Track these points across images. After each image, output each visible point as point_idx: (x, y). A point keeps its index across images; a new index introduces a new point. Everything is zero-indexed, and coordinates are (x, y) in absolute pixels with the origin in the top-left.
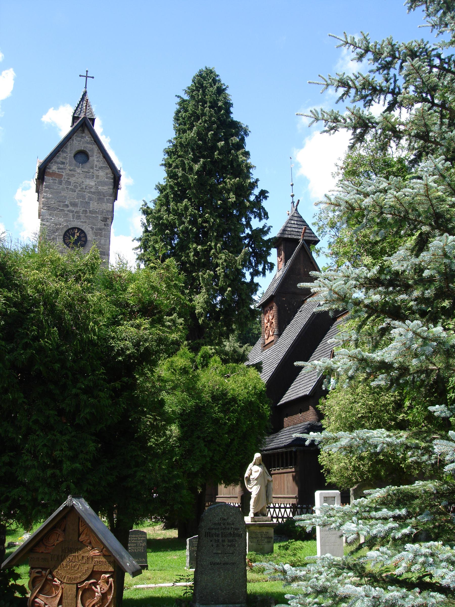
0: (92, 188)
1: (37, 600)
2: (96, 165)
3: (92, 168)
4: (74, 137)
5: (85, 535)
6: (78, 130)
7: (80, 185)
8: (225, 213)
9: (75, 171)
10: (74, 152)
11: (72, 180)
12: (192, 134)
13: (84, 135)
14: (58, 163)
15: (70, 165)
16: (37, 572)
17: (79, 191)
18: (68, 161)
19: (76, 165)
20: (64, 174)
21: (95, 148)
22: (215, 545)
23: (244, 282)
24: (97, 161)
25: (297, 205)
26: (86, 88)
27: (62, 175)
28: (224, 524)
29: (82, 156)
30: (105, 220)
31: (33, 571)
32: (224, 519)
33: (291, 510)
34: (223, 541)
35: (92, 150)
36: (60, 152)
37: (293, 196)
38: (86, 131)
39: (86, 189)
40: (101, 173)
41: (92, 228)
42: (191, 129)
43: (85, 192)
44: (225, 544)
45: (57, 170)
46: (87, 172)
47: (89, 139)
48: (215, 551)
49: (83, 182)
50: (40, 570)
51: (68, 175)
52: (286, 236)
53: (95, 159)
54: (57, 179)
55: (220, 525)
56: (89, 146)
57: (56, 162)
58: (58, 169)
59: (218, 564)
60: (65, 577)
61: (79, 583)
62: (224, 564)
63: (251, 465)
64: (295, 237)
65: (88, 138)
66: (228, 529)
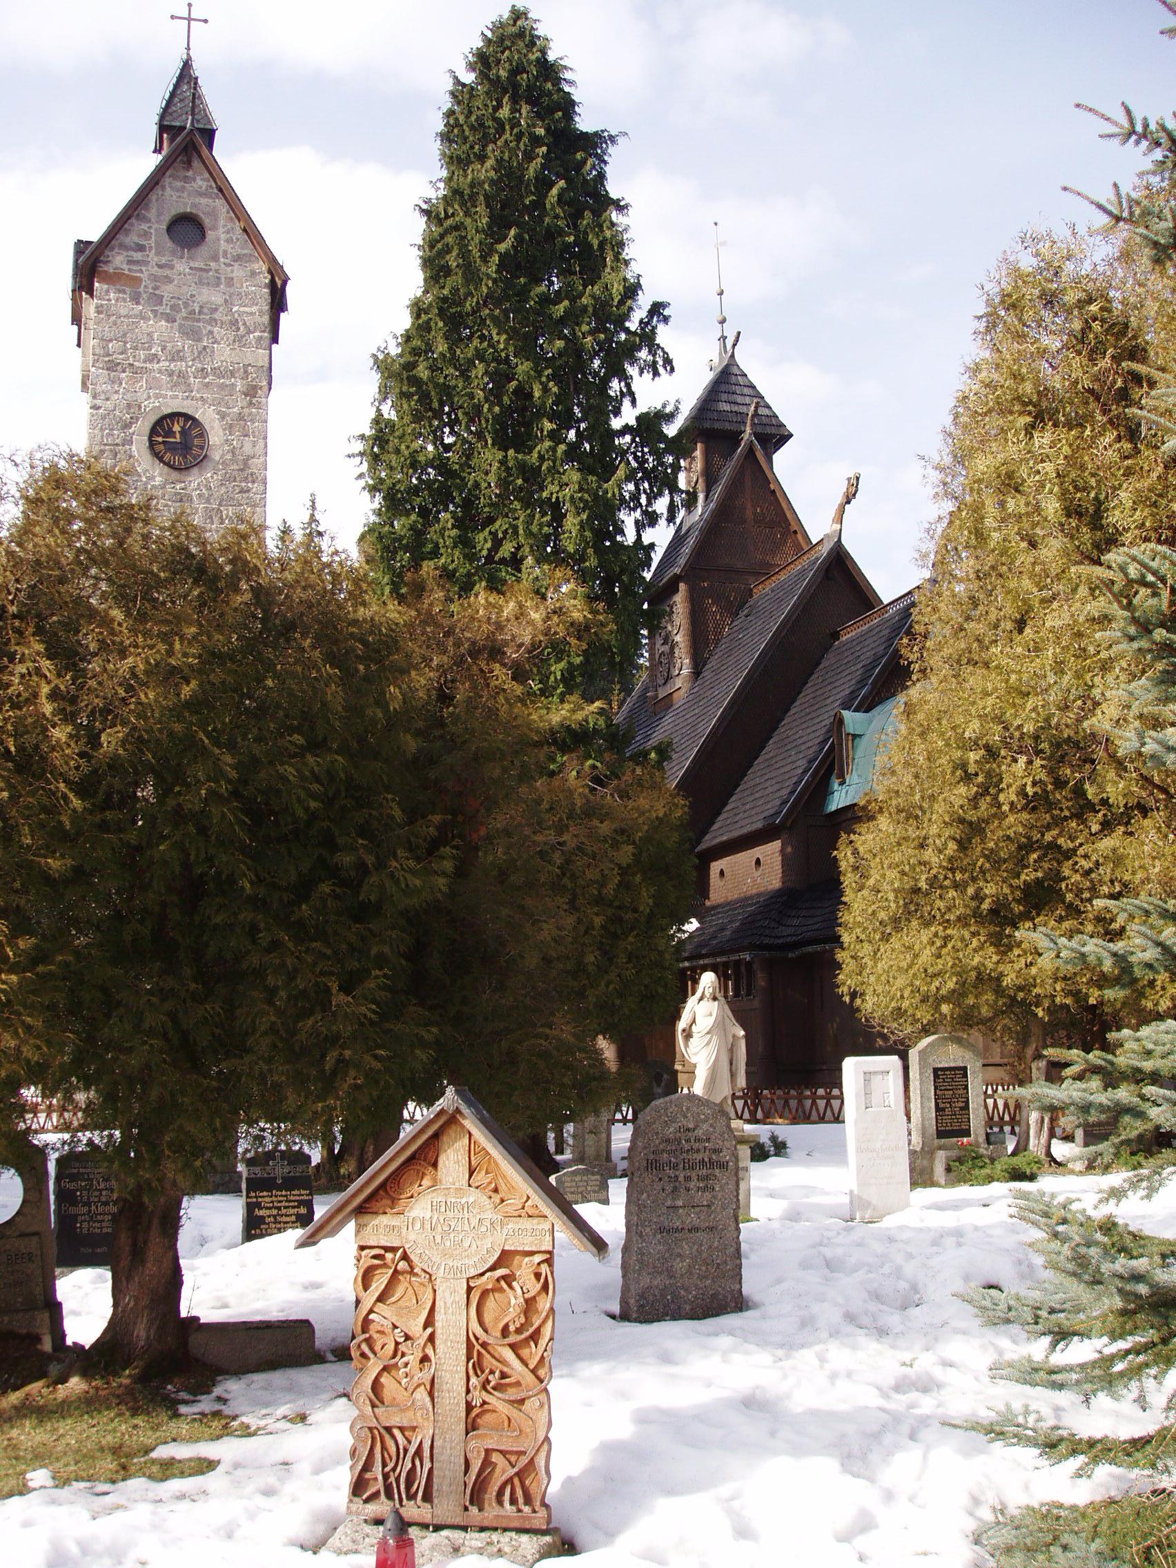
0: (216, 310)
1: (372, 1316)
2: (225, 252)
3: (215, 258)
4: (167, 181)
5: (483, 1172)
6: (174, 161)
7: (186, 305)
8: (570, 368)
9: (172, 267)
10: (167, 218)
11: (167, 291)
12: (485, 171)
13: (190, 174)
14: (127, 248)
15: (158, 253)
16: (374, 1257)
17: (185, 319)
18: (152, 242)
19: (173, 253)
20: (144, 276)
21: (220, 203)
22: (669, 1188)
23: (621, 545)
24: (227, 241)
25: (734, 345)
26: (188, 49)
27: (139, 280)
28: (688, 1141)
29: (187, 230)
30: (251, 392)
31: (364, 1253)
32: (688, 1130)
33: (746, 1103)
34: (688, 1179)
35: (213, 214)
36: (133, 220)
37: (723, 322)
38: (196, 163)
39: (200, 313)
40: (238, 272)
41: (223, 416)
42: (482, 158)
43: (199, 321)
44: (692, 1185)
45: (125, 267)
46: (201, 270)
47: (204, 184)
48: (669, 1203)
49: (192, 296)
50: (382, 1252)
51: (155, 278)
52: (707, 425)
53: (223, 236)
54: (128, 290)
55: (679, 1143)
56: (204, 201)
57: (122, 246)
58: (130, 262)
59: (677, 1230)
60: (440, 1264)
61: (473, 1278)
62: (690, 1231)
63: (692, 1002)
64: (727, 426)
65: (201, 182)
66: (698, 1151)
